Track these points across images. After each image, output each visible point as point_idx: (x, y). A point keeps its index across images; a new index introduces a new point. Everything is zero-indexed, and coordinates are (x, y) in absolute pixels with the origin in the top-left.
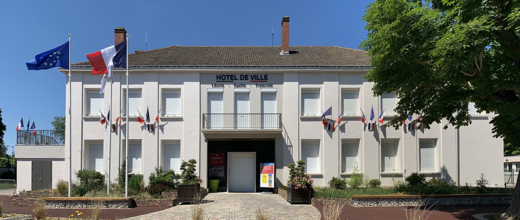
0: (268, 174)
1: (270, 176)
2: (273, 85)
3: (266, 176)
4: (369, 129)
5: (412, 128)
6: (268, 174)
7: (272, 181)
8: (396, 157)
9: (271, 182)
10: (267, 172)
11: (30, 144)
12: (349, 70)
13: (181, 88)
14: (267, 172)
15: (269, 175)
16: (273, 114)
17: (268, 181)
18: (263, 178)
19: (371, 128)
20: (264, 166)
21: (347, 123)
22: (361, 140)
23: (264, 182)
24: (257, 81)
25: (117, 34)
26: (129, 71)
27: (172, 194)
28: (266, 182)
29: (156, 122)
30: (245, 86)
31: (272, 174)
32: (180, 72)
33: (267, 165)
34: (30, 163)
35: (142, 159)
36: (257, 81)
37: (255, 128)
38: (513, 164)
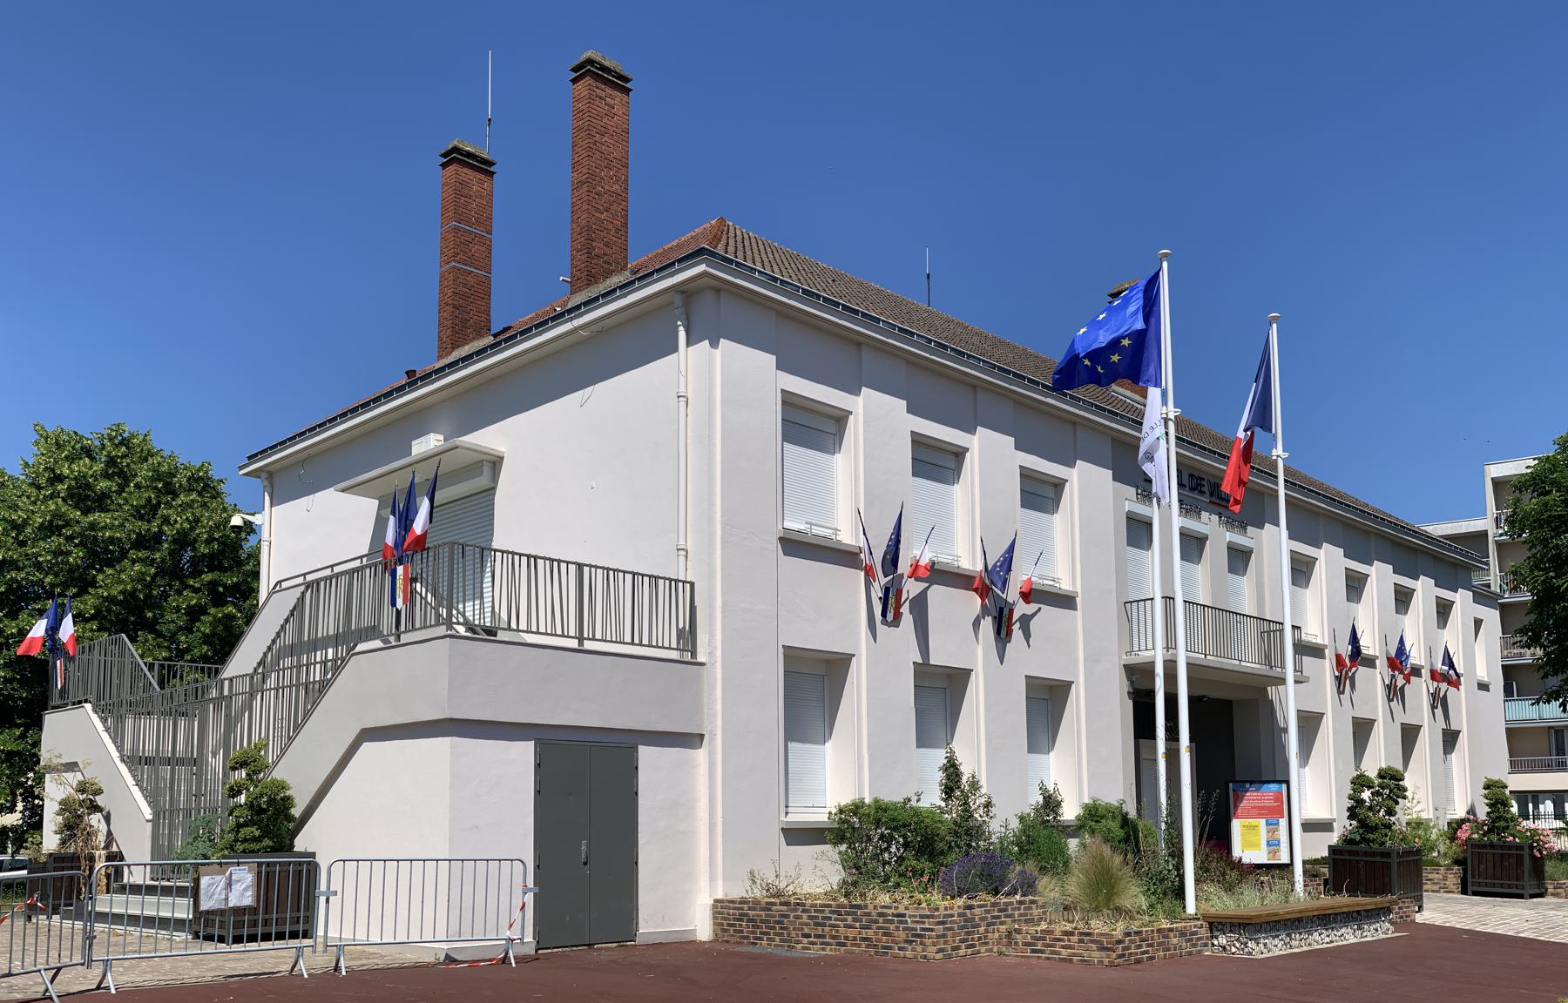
0: (1263, 822)
1: (1271, 824)
2: (1249, 528)
3: (1257, 826)
6: (1264, 820)
7: (1279, 841)
8: (1052, 754)
9: (1279, 845)
10: (1259, 814)
11: (398, 638)
13: (1067, 481)
15: (1268, 824)
16: (1145, 600)
17: (1264, 842)
18: (1243, 834)
19: (892, 611)
20: (1247, 791)
23: (1247, 844)
24: (1218, 501)
26: (1225, 468)
27: (928, 917)
28: (1255, 845)
29: (1393, 676)
32: (1053, 411)
33: (1257, 790)
35: (711, 754)
36: (1218, 501)
37: (1224, 660)
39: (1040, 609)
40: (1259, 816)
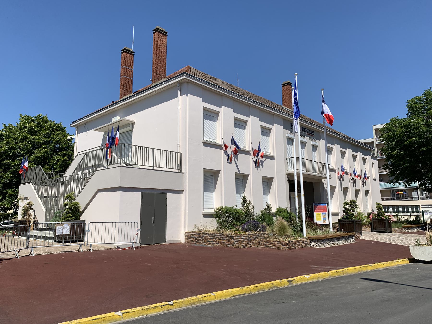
0: (322, 213)
4: (227, 161)
5: (230, 159)
7: (326, 219)
9: (326, 219)
12: (240, 99)
14: (321, 211)
17: (322, 218)
18: (317, 216)
19: (230, 160)
20: (317, 205)
21: (265, 161)
22: (249, 175)
24: (309, 134)
25: (160, 34)
28: (320, 219)
30: (316, 140)
31: (326, 213)
33: (320, 205)
34: (138, 195)
36: (309, 134)
37: (311, 173)
38: (399, 207)
39: (266, 160)
40: (321, 212)
